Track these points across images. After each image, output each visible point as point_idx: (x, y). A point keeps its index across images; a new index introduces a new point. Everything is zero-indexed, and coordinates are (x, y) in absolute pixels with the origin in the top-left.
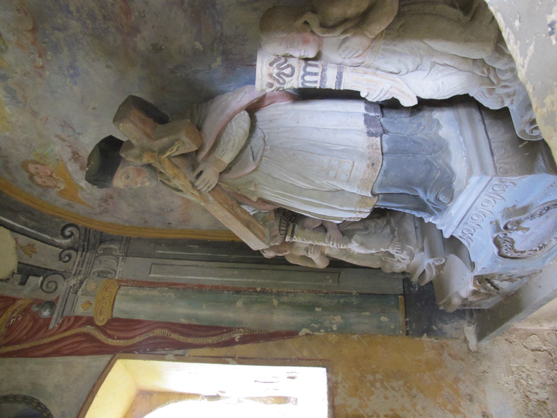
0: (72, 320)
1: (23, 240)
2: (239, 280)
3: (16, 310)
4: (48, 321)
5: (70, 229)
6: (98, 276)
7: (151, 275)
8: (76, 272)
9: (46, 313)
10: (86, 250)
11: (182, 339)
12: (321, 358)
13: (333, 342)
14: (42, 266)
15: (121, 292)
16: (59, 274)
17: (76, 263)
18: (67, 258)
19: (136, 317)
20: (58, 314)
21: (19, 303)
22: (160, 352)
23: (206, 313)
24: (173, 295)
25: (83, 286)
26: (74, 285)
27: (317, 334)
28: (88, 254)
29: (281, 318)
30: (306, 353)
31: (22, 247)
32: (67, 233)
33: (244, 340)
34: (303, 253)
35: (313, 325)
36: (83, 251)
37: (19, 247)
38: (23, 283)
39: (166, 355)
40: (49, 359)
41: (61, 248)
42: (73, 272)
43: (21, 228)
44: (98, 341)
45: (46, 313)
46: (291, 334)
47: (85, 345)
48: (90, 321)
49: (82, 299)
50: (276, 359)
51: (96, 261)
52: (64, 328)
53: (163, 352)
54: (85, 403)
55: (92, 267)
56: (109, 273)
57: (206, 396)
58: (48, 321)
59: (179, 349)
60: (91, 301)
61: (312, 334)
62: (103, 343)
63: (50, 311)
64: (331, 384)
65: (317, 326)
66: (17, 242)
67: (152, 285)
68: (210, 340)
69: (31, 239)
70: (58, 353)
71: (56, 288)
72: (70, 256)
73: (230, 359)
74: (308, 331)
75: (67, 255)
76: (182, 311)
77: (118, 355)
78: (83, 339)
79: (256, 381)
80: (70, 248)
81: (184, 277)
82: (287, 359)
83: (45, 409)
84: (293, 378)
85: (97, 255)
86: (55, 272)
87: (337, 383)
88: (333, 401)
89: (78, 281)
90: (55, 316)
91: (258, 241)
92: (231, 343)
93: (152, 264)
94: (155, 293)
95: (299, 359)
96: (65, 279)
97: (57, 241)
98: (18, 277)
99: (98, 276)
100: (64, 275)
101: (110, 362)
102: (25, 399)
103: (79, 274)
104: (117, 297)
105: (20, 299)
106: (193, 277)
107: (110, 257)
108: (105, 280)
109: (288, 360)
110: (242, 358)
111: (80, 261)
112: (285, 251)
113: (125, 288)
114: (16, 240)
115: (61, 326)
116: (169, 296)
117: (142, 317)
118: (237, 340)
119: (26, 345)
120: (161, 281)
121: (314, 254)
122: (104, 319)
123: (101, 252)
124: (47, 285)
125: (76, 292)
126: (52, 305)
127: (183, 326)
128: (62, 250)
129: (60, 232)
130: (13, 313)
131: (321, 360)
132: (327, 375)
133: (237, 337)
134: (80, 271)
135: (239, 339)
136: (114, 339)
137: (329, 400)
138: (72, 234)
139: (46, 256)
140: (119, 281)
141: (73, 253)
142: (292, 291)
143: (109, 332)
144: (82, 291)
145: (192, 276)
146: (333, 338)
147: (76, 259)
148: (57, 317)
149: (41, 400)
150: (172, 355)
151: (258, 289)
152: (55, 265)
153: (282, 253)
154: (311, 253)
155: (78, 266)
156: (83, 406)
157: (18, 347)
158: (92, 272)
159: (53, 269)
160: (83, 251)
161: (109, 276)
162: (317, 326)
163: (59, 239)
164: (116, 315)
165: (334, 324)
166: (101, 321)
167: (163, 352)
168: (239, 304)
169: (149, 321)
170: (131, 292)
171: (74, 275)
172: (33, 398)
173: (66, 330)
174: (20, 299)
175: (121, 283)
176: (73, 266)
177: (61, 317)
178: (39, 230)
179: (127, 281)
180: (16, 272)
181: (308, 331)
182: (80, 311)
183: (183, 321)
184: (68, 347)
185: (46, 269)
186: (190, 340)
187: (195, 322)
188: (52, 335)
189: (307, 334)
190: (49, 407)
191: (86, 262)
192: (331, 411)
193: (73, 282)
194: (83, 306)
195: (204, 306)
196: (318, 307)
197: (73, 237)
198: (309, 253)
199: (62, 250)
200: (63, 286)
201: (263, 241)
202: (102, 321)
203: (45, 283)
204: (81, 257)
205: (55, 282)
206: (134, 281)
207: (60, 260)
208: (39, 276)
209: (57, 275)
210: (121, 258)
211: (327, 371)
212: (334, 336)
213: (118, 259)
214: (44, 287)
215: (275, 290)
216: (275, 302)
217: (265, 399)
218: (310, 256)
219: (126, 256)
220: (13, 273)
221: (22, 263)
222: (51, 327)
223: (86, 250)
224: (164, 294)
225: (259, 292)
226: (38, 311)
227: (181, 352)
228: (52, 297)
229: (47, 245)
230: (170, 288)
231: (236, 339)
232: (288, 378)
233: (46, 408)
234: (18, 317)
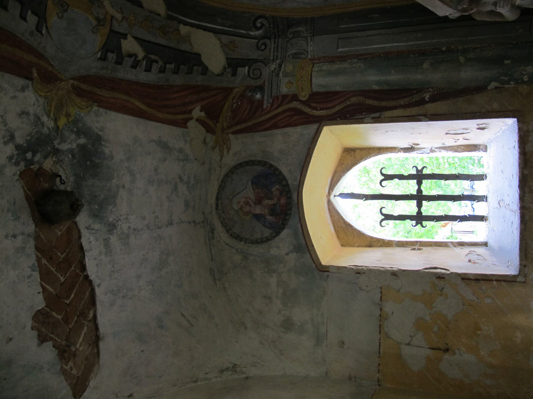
0: (280, 98)
1: (225, 39)
2: (423, 42)
3: (234, 97)
4: (261, 102)
5: (259, 21)
6: (293, 58)
7: (340, 50)
8: (274, 57)
9: (258, 96)
10: (277, 37)
11: (376, 103)
12: (511, 109)
13: (524, 93)
14: (245, 58)
15: (315, 69)
16: (260, 62)
17: (272, 50)
18: (263, 47)
19: (333, 89)
20: (268, 96)
21: (235, 90)
22: (359, 117)
23: (395, 77)
24: (362, 65)
25: (282, 69)
26: (275, 69)
27: (506, 86)
28: (280, 40)
29: (468, 75)
30: (495, 106)
31: (225, 45)
32: (259, 25)
33: (433, 99)
34: (490, 8)
35: (503, 78)
36: (275, 38)
37: (224, 46)
38: (234, 74)
39: (364, 118)
40: (270, 132)
41: (256, 39)
42: (272, 58)
43: (220, 29)
44: (305, 113)
45: (258, 96)
46: (481, 89)
47: (295, 118)
48: (295, 98)
49: (285, 81)
50: (465, 113)
51: (288, 45)
52: (275, 106)
53: (361, 117)
54: (305, 162)
55: (286, 51)
56: (302, 54)
57: (402, 149)
58: (261, 102)
59: (375, 112)
60: (292, 81)
61: (502, 87)
62: (309, 115)
63: (261, 94)
64: (522, 133)
65: (506, 79)
66: (221, 41)
67: (342, 58)
68: (402, 102)
69: (231, 37)
70: (275, 126)
71: (261, 74)
72: (265, 44)
73: (423, 117)
74: (497, 84)
75: (263, 44)
76: (373, 78)
77: (323, 123)
78: (293, 113)
79: (447, 134)
80: (263, 37)
81: (370, 47)
82: (477, 113)
83: (276, 169)
84: (483, 129)
85: (288, 39)
86: (256, 61)
87: (528, 131)
88: (524, 148)
89: (277, 65)
90: (266, 97)
91: (445, 7)
92: (422, 102)
93: (339, 39)
94: (346, 65)
95: (489, 112)
96: (266, 65)
97: (252, 33)
98: (229, 70)
99: (293, 58)
100: (265, 62)
101: (318, 129)
102: (260, 163)
103: (277, 59)
104: (313, 74)
105: (235, 88)
106: (379, 46)
107: (300, 39)
108: (300, 60)
109: (478, 114)
110: (432, 115)
111: (274, 48)
112: (472, 9)
113: (318, 65)
114: (219, 39)
115: (272, 105)
116: (359, 66)
117: (338, 89)
118: (427, 100)
119: (250, 123)
120: (349, 54)
121: (503, 7)
122: (306, 94)
123: (290, 36)
124: (253, 72)
125: (278, 75)
126: (261, 88)
127: (376, 91)
128: (257, 40)
129: (252, 25)
130: (233, 99)
131: (511, 111)
132: (518, 125)
133: (427, 96)
134: (277, 56)
135: (428, 98)
136: (317, 110)
137: (520, 147)
138: (263, 25)
139: (246, 48)
140: (311, 60)
141: (266, 40)
142: (479, 46)
143: (312, 105)
144: (283, 73)
145: (378, 45)
146: (524, 89)
147: (271, 46)
148: (268, 98)
149: (272, 163)
150: (369, 119)
151: (444, 49)
152: (255, 55)
153: (468, 11)
154: (500, 7)
155: (274, 52)
156: (304, 164)
157: (244, 126)
158: (287, 56)
159: (254, 58)
160: (275, 38)
161: (302, 56)
162: (506, 79)
163: (253, 31)
164: (315, 89)
165: (524, 75)
166: (304, 96)
167: (361, 117)
168: (426, 65)
169: (345, 91)
170: (324, 68)
171: (273, 60)
172: (266, 162)
173: (277, 108)
174: (235, 88)
175: (314, 61)
176: (270, 53)
177: (271, 98)
178: (235, 28)
179: (319, 59)
180: (227, 66)
181: (497, 84)
182: (284, 90)
183: (375, 87)
184: (282, 121)
185: (249, 59)
186: (384, 104)
187: (386, 87)
188: (267, 113)
189: (496, 88)
190: (279, 168)
191: (280, 48)
192: (522, 157)
193: (273, 67)
194: (286, 86)
195: (393, 72)
196: (507, 60)
197: (264, 28)
198: (498, 8)
199: (257, 40)
200: (266, 72)
201: (450, 7)
202: (304, 97)
203: (251, 71)
204: (275, 43)
205: (259, 70)
206: (325, 57)
207: (258, 49)
208: (245, 66)
209: (258, 63)
210: (309, 39)
211: (518, 121)
212: (525, 87)
213: (307, 40)
214: (251, 75)
215: (460, 48)
216: (462, 59)
217: (456, 148)
218: (499, 10)
219: (314, 36)
220: (225, 68)
221: (230, 59)
222: (265, 107)
223: (277, 37)
224: (354, 65)
225: (445, 51)
226: (251, 96)
227: (377, 115)
228: (259, 82)
229: (245, 39)
230: (359, 59)
231: (426, 98)
232: (478, 129)
233: (277, 168)
234: (238, 102)
